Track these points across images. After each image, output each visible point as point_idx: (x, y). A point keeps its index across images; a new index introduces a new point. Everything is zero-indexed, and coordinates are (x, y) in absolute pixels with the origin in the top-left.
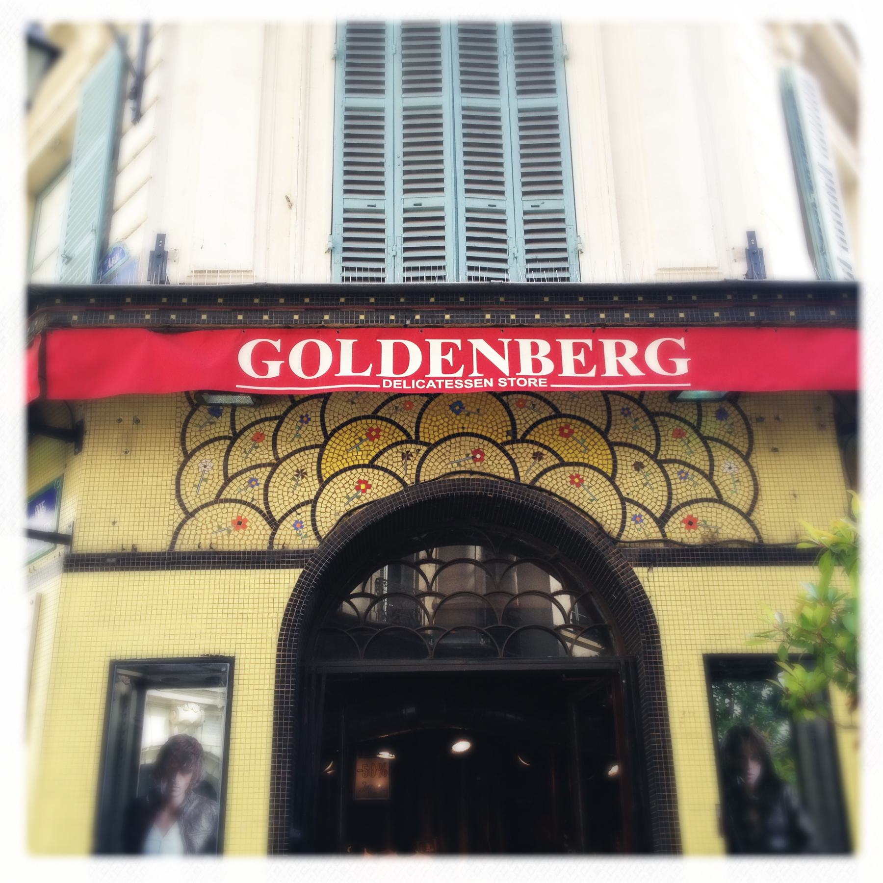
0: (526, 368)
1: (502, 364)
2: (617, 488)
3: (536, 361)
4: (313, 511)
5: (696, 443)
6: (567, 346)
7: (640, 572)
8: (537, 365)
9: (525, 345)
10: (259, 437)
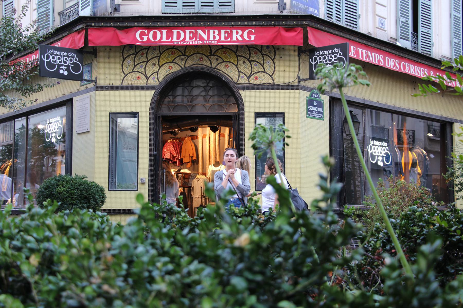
0: (211, 38)
1: (205, 37)
2: (238, 68)
3: (214, 36)
4: (157, 74)
5: (260, 56)
6: (223, 31)
7: (241, 92)
8: (214, 37)
9: (212, 31)
10: (143, 54)
